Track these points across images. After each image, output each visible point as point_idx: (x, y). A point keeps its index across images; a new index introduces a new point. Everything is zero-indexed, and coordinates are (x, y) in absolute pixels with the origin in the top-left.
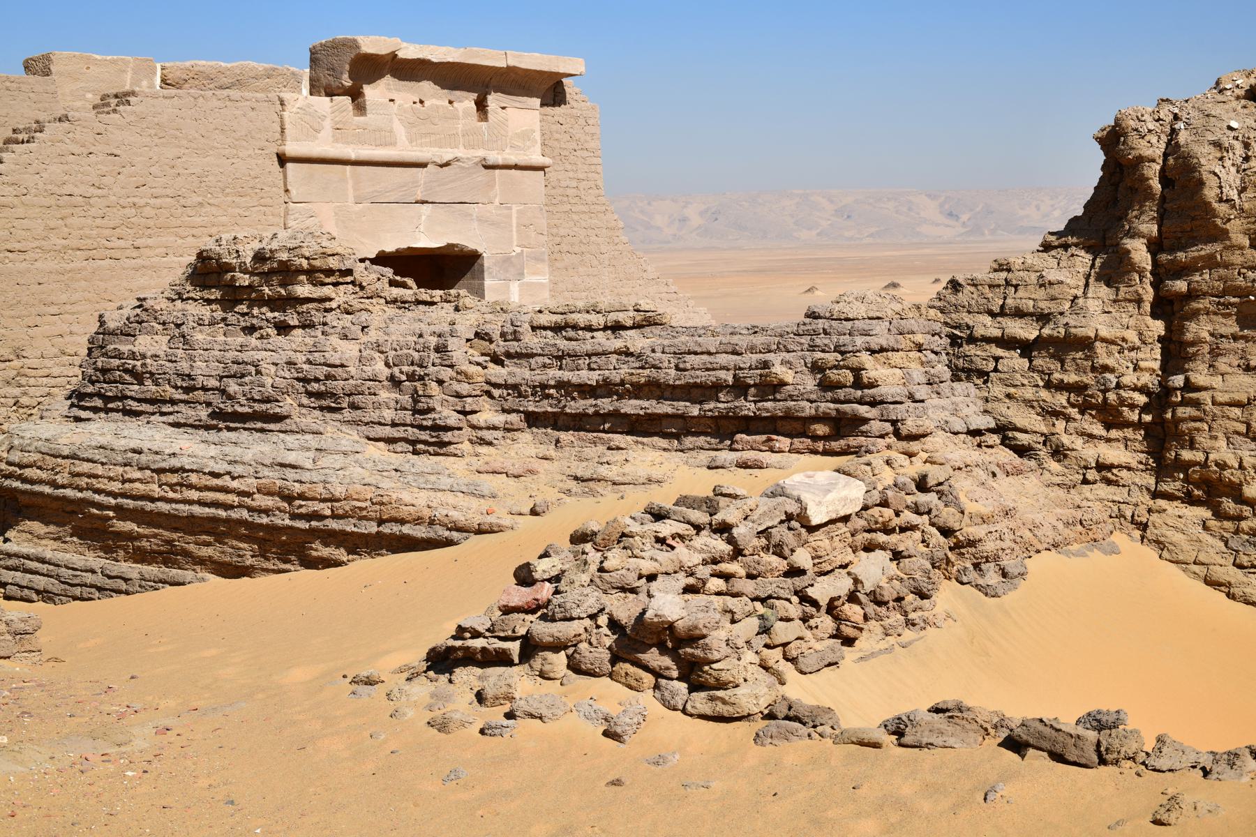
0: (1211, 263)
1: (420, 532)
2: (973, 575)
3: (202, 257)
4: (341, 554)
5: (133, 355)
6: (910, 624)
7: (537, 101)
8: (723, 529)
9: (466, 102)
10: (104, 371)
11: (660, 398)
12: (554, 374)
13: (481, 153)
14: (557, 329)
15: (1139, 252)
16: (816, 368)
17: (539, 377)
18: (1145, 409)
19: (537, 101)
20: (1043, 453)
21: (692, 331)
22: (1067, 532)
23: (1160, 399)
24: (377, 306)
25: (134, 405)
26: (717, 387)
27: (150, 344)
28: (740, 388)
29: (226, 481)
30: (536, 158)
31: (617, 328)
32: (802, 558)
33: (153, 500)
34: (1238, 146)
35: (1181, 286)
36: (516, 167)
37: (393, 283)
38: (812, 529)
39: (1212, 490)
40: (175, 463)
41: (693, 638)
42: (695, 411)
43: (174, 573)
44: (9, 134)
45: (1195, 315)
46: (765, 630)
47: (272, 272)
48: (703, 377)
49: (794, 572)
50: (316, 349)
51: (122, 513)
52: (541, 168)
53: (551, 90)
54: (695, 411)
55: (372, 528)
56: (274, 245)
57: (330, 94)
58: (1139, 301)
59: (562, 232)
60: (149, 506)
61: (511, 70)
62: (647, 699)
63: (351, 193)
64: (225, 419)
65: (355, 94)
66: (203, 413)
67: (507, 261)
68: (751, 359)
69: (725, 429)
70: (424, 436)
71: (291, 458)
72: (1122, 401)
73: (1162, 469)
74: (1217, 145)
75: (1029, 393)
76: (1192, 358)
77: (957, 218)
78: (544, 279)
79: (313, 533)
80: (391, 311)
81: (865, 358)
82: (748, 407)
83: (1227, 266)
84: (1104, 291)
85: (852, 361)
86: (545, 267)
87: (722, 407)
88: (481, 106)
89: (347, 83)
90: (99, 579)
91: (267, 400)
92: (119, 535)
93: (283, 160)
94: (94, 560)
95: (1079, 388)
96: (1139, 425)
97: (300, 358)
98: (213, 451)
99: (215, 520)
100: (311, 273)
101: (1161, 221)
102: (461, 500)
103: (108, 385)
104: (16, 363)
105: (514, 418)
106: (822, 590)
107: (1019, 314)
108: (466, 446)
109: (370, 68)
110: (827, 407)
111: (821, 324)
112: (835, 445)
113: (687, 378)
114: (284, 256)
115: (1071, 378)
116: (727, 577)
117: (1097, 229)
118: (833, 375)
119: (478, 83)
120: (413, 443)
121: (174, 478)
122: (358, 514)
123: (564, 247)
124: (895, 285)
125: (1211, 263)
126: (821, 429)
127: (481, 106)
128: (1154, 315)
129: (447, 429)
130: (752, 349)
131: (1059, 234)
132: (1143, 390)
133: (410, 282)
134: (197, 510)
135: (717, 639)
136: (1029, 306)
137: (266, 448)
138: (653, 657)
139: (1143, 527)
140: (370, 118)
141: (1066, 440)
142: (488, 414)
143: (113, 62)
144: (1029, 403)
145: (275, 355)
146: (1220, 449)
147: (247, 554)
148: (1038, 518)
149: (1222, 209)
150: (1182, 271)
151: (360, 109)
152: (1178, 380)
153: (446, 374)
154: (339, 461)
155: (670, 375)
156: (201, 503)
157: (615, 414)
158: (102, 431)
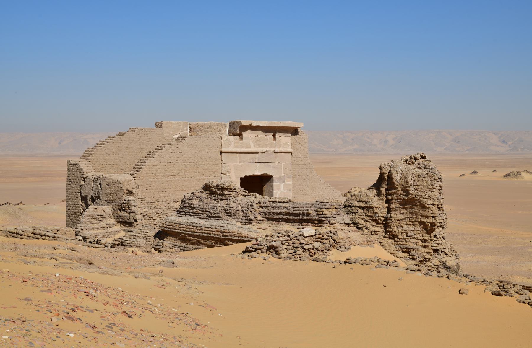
0: (395, 193)
1: (246, 239)
2: (339, 248)
3: (206, 185)
4: (231, 243)
5: (191, 204)
6: (324, 255)
7: (290, 134)
8: (289, 236)
9: (270, 135)
10: (185, 207)
11: (290, 216)
12: (272, 211)
13: (273, 149)
14: (273, 202)
15: (383, 191)
16: (316, 211)
17: (269, 211)
18: (384, 221)
19: (290, 134)
20: (364, 228)
21: (297, 204)
22: (363, 243)
23: (386, 219)
24: (240, 196)
25: (191, 214)
26: (299, 214)
27: (195, 202)
28: (303, 214)
29: (210, 229)
30: (289, 150)
31: (284, 202)
32: (303, 242)
33: (195, 232)
34: (401, 172)
35: (390, 197)
36: (283, 152)
37: (243, 191)
38: (305, 237)
39: (393, 236)
40: (200, 225)
41: (277, 248)
42: (296, 218)
43: (199, 247)
44: (156, 147)
45: (392, 203)
46: (295, 252)
47: (220, 189)
48: (297, 212)
49: (301, 244)
50: (228, 204)
51: (189, 235)
52: (291, 153)
53: (294, 131)
54: (296, 218)
55: (237, 238)
56: (221, 183)
57: (234, 135)
58: (383, 200)
59: (296, 170)
60: (194, 234)
61: (282, 127)
62: (271, 256)
63: (238, 161)
64: (210, 217)
65: (240, 135)
66: (205, 216)
67: (280, 178)
68: (306, 209)
69: (301, 222)
70: (248, 221)
71: (222, 225)
72: (379, 219)
73: (386, 232)
74: (397, 171)
75: (362, 217)
76: (391, 211)
77: (507, 143)
78: (291, 183)
79: (226, 239)
80: (243, 197)
81: (324, 210)
82: (304, 218)
83: (398, 194)
84: (377, 198)
85: (322, 210)
86: (291, 180)
87: (300, 218)
88: (274, 136)
89: (238, 132)
90: (184, 248)
91: (218, 214)
92: (188, 239)
93: (221, 153)
94: (182, 244)
95: (371, 216)
96: (382, 224)
97: (225, 206)
98: (207, 223)
99: (207, 236)
100: (227, 189)
101: (387, 185)
102: (253, 233)
103: (185, 209)
104: (157, 203)
105: (264, 219)
106: (306, 247)
107: (362, 202)
108: (255, 224)
109: (244, 128)
110: (317, 218)
111: (318, 203)
112: (319, 225)
113: (295, 212)
114: (222, 186)
115: (370, 214)
116: (289, 243)
117: (377, 186)
118: (318, 212)
119: (273, 131)
120: (245, 223)
121: (200, 228)
122: (235, 236)
123: (297, 174)
124: (476, 172)
125: (395, 193)
126: (316, 222)
127: (274, 136)
128: (386, 203)
129: (252, 220)
130: (306, 207)
131: (371, 186)
132: (383, 217)
133: (247, 191)
134: (204, 234)
135: (280, 249)
136: (364, 200)
137: (218, 223)
138: (272, 250)
139: (381, 243)
140: (244, 141)
141: (368, 226)
142: (260, 218)
143: (178, 123)
144: (362, 219)
145: (220, 205)
146: (395, 229)
147: (213, 243)
148: (356, 239)
149: (396, 183)
150: (390, 195)
151: (241, 138)
152: (389, 215)
153: (252, 210)
154: (231, 226)
155: (292, 212)
156: (205, 233)
157: (282, 218)
158: (184, 219)
